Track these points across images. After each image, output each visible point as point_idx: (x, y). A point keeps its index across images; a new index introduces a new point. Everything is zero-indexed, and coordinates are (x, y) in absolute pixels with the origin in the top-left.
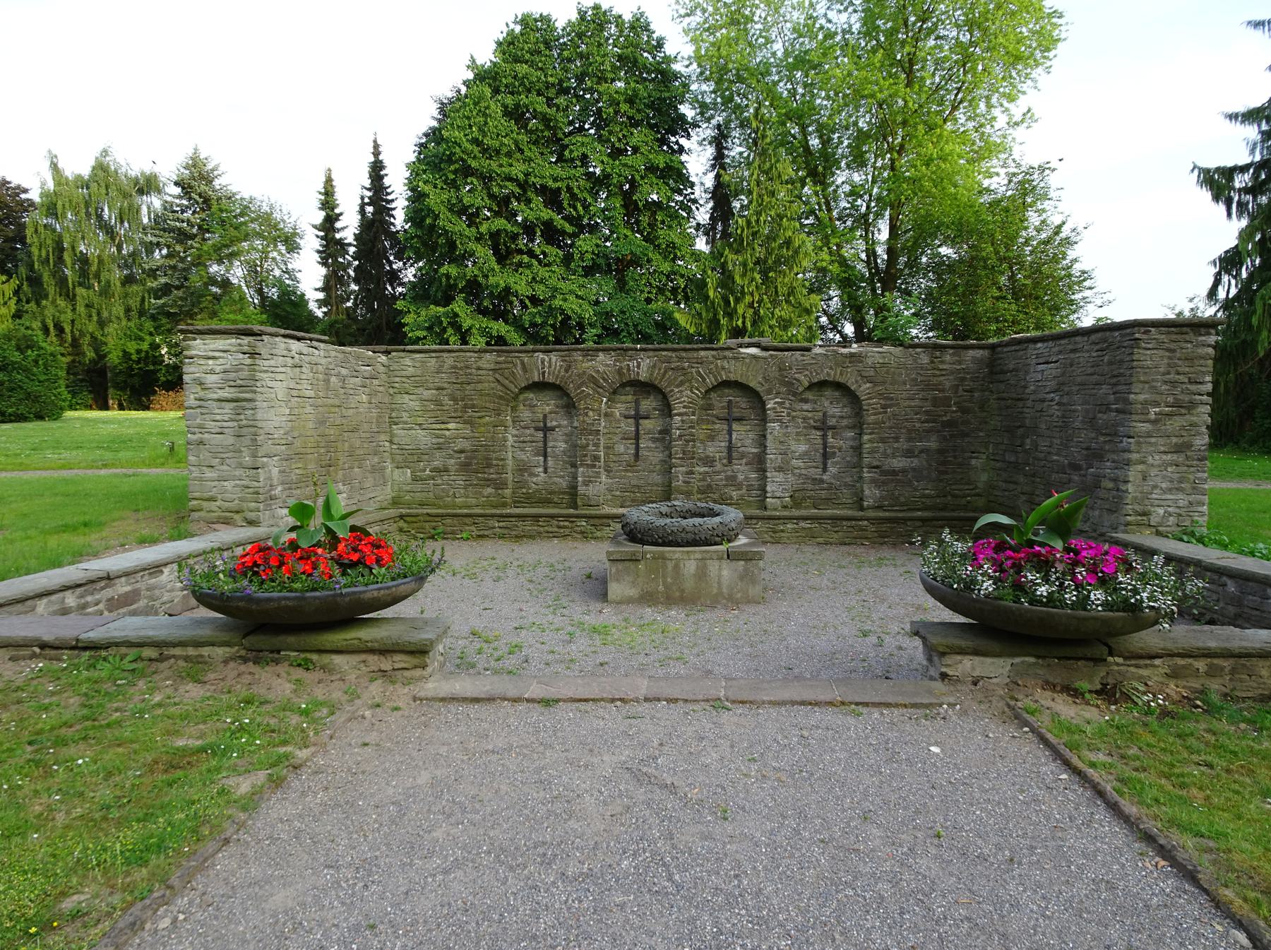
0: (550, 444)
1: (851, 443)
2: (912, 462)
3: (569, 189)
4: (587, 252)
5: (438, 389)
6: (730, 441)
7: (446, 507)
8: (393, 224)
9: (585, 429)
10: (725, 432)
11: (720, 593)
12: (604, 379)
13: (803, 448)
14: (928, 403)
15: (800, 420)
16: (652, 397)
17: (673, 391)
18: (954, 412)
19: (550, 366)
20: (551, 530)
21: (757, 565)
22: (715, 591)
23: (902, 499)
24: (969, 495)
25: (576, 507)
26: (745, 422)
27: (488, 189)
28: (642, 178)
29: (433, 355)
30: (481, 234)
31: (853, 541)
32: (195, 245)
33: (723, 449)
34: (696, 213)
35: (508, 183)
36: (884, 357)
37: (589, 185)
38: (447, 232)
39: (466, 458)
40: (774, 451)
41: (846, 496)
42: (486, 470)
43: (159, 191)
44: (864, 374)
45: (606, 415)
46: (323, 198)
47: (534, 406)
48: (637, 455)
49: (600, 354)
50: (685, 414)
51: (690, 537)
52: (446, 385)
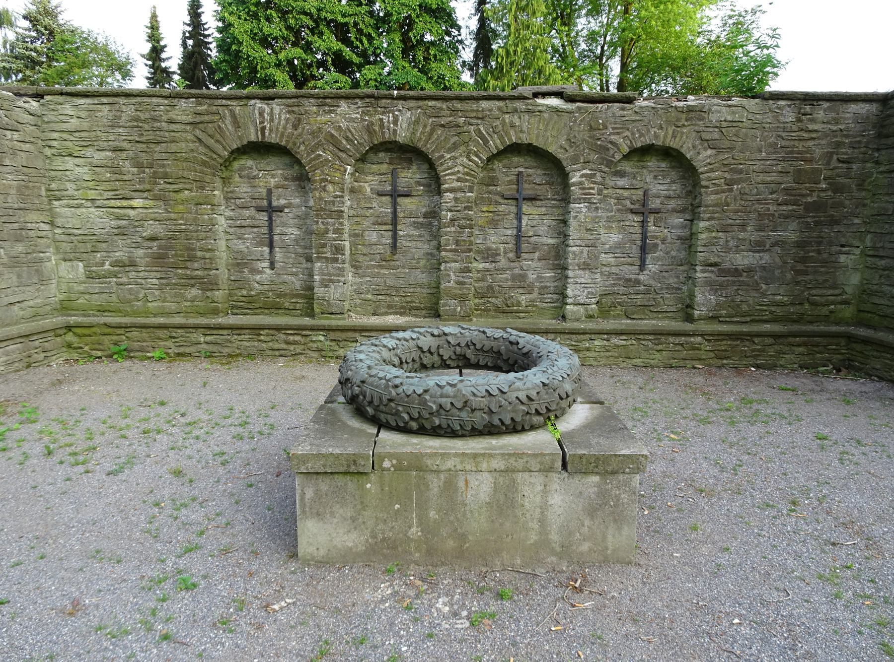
0: (278, 230)
1: (679, 232)
2: (761, 258)
3: (356, 24)
4: (371, 79)
5: (115, 150)
6: (519, 229)
7: (136, 314)
8: (209, 55)
9: (322, 209)
10: (512, 215)
11: (544, 543)
12: (347, 139)
13: (615, 238)
14: (789, 178)
15: (613, 201)
16: (414, 167)
17: (442, 157)
18: (823, 190)
19: (272, 120)
20: (276, 346)
21: (627, 483)
22: (533, 537)
23: (745, 307)
24: (832, 303)
25: (312, 315)
26: (538, 203)
27: (286, 21)
28: (418, 17)
29: (105, 100)
30: (280, 61)
31: (682, 363)
32: (42, 70)
33: (509, 239)
34: (463, 52)
35: (302, 16)
36: (734, 113)
37: (373, 22)
38: (249, 56)
39: (160, 248)
40: (578, 242)
41: (669, 302)
42: (189, 264)
43: (11, 24)
44: (705, 136)
45: (352, 191)
46: (149, 31)
47: (254, 177)
48: (394, 246)
49: (342, 103)
50: (460, 190)
51: (480, 419)
52: (125, 145)
